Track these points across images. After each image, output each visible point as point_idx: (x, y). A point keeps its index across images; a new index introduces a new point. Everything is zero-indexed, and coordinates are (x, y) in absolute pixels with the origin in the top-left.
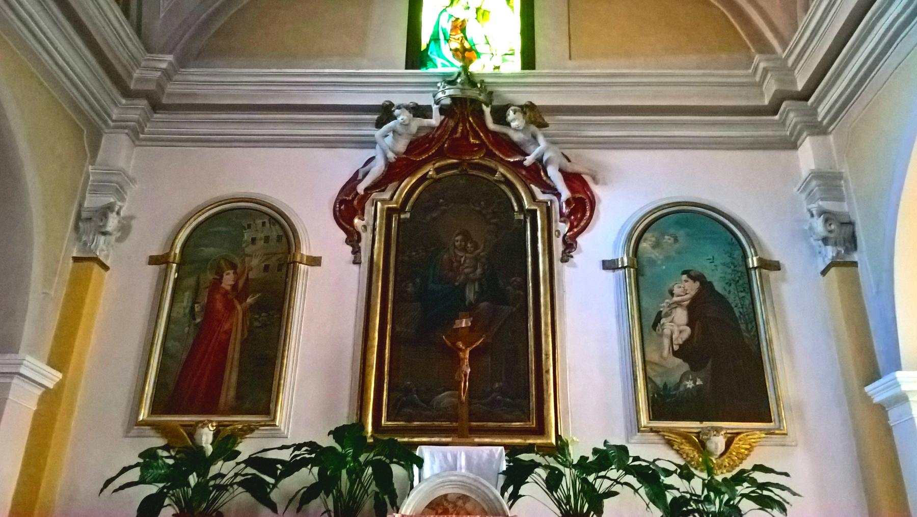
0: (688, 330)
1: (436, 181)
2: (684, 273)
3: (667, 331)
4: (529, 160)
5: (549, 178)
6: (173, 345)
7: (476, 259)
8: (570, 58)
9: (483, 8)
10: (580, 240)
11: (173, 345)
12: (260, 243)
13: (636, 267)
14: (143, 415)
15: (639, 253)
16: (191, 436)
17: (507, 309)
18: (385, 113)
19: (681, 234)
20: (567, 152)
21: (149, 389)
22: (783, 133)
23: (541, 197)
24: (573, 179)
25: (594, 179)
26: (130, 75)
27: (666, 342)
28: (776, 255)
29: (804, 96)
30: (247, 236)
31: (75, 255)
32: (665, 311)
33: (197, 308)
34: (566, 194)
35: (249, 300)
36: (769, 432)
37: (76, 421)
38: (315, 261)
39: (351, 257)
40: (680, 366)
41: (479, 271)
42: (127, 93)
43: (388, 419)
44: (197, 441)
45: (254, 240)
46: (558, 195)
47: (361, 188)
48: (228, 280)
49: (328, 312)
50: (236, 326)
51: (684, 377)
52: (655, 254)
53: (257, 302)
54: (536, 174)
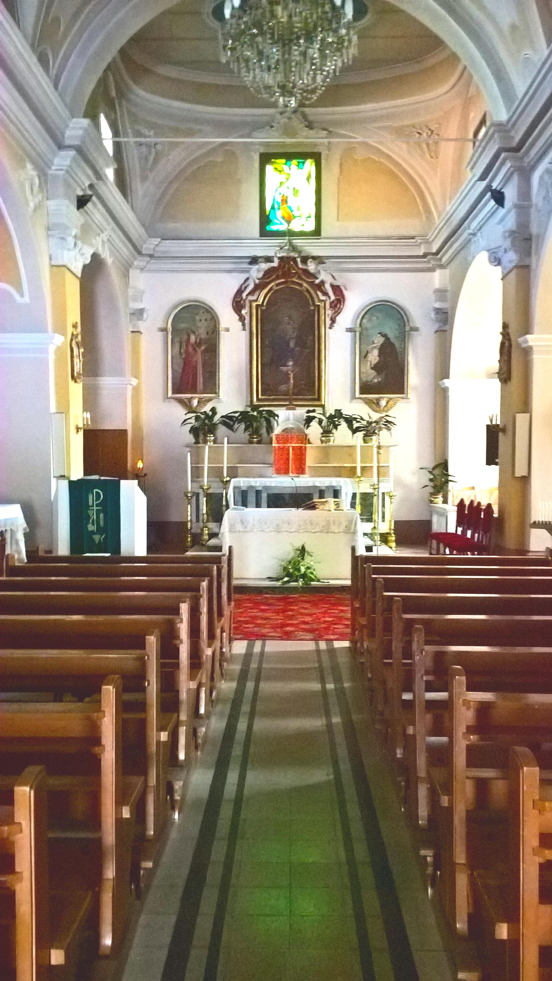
0: (378, 358)
1: (276, 291)
2: (379, 333)
3: (369, 359)
4: (317, 281)
5: (326, 289)
6: (176, 367)
7: (294, 328)
8: (338, 220)
9: (296, 189)
10: (337, 318)
11: (176, 367)
12: (203, 321)
13: (360, 333)
14: (170, 394)
15: (362, 324)
16: (190, 402)
17: (307, 351)
18: (254, 260)
19: (379, 315)
20: (334, 274)
21: (170, 385)
22: (428, 266)
23: (322, 298)
24: (337, 289)
25: (346, 289)
26: (142, 247)
27: (369, 363)
28: (418, 325)
29: (517, 149)
30: (198, 318)
31: (131, 330)
32: (370, 350)
33: (182, 351)
34: (333, 297)
35: (203, 348)
36: (402, 398)
37: (144, 396)
38: (227, 330)
39: (241, 327)
40: (373, 373)
41: (295, 334)
42: (140, 253)
43: (262, 395)
44: (192, 403)
45: (200, 320)
46: (330, 298)
47: (244, 295)
48: (193, 338)
49: (235, 349)
50: (199, 358)
51: (374, 378)
52: (369, 326)
53: (205, 349)
54: (320, 287)
